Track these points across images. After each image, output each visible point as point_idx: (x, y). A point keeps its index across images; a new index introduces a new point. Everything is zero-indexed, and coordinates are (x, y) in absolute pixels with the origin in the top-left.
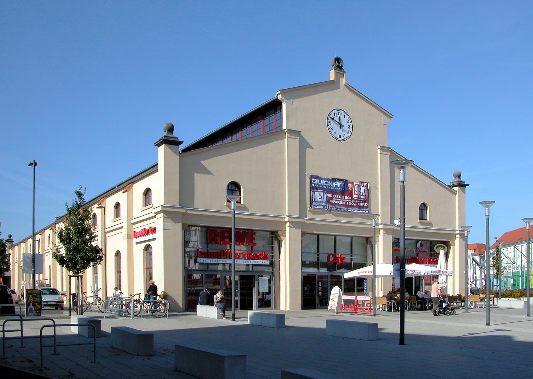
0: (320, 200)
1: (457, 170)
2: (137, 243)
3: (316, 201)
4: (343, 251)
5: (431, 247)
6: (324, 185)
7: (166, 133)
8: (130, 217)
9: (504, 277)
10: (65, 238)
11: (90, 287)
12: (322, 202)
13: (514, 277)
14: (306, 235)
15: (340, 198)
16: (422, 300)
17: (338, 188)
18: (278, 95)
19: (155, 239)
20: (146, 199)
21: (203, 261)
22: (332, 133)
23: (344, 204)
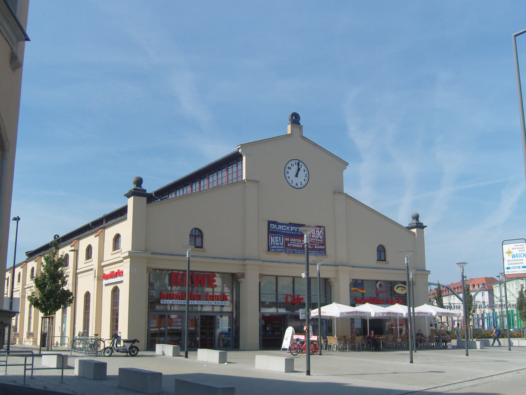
0: (278, 244)
1: (416, 211)
2: (106, 285)
3: (274, 244)
4: (302, 291)
5: (391, 287)
6: (281, 230)
7: (135, 186)
8: (101, 259)
9: (500, 316)
10: (40, 284)
11: (58, 328)
12: (280, 245)
13: (500, 317)
14: (264, 277)
15: (297, 242)
16: (370, 340)
17: (295, 232)
18: (239, 149)
19: (122, 282)
20: (115, 243)
21: (166, 302)
22: (291, 179)
23: (301, 247)
